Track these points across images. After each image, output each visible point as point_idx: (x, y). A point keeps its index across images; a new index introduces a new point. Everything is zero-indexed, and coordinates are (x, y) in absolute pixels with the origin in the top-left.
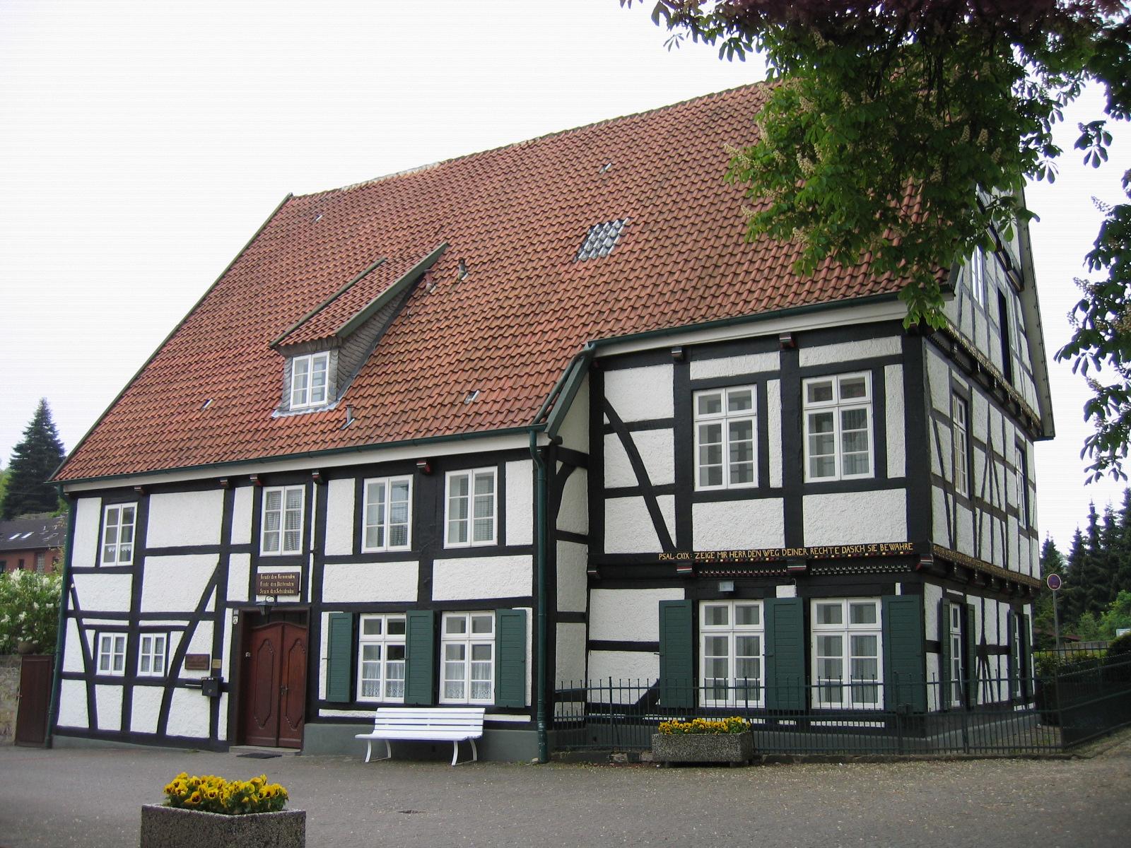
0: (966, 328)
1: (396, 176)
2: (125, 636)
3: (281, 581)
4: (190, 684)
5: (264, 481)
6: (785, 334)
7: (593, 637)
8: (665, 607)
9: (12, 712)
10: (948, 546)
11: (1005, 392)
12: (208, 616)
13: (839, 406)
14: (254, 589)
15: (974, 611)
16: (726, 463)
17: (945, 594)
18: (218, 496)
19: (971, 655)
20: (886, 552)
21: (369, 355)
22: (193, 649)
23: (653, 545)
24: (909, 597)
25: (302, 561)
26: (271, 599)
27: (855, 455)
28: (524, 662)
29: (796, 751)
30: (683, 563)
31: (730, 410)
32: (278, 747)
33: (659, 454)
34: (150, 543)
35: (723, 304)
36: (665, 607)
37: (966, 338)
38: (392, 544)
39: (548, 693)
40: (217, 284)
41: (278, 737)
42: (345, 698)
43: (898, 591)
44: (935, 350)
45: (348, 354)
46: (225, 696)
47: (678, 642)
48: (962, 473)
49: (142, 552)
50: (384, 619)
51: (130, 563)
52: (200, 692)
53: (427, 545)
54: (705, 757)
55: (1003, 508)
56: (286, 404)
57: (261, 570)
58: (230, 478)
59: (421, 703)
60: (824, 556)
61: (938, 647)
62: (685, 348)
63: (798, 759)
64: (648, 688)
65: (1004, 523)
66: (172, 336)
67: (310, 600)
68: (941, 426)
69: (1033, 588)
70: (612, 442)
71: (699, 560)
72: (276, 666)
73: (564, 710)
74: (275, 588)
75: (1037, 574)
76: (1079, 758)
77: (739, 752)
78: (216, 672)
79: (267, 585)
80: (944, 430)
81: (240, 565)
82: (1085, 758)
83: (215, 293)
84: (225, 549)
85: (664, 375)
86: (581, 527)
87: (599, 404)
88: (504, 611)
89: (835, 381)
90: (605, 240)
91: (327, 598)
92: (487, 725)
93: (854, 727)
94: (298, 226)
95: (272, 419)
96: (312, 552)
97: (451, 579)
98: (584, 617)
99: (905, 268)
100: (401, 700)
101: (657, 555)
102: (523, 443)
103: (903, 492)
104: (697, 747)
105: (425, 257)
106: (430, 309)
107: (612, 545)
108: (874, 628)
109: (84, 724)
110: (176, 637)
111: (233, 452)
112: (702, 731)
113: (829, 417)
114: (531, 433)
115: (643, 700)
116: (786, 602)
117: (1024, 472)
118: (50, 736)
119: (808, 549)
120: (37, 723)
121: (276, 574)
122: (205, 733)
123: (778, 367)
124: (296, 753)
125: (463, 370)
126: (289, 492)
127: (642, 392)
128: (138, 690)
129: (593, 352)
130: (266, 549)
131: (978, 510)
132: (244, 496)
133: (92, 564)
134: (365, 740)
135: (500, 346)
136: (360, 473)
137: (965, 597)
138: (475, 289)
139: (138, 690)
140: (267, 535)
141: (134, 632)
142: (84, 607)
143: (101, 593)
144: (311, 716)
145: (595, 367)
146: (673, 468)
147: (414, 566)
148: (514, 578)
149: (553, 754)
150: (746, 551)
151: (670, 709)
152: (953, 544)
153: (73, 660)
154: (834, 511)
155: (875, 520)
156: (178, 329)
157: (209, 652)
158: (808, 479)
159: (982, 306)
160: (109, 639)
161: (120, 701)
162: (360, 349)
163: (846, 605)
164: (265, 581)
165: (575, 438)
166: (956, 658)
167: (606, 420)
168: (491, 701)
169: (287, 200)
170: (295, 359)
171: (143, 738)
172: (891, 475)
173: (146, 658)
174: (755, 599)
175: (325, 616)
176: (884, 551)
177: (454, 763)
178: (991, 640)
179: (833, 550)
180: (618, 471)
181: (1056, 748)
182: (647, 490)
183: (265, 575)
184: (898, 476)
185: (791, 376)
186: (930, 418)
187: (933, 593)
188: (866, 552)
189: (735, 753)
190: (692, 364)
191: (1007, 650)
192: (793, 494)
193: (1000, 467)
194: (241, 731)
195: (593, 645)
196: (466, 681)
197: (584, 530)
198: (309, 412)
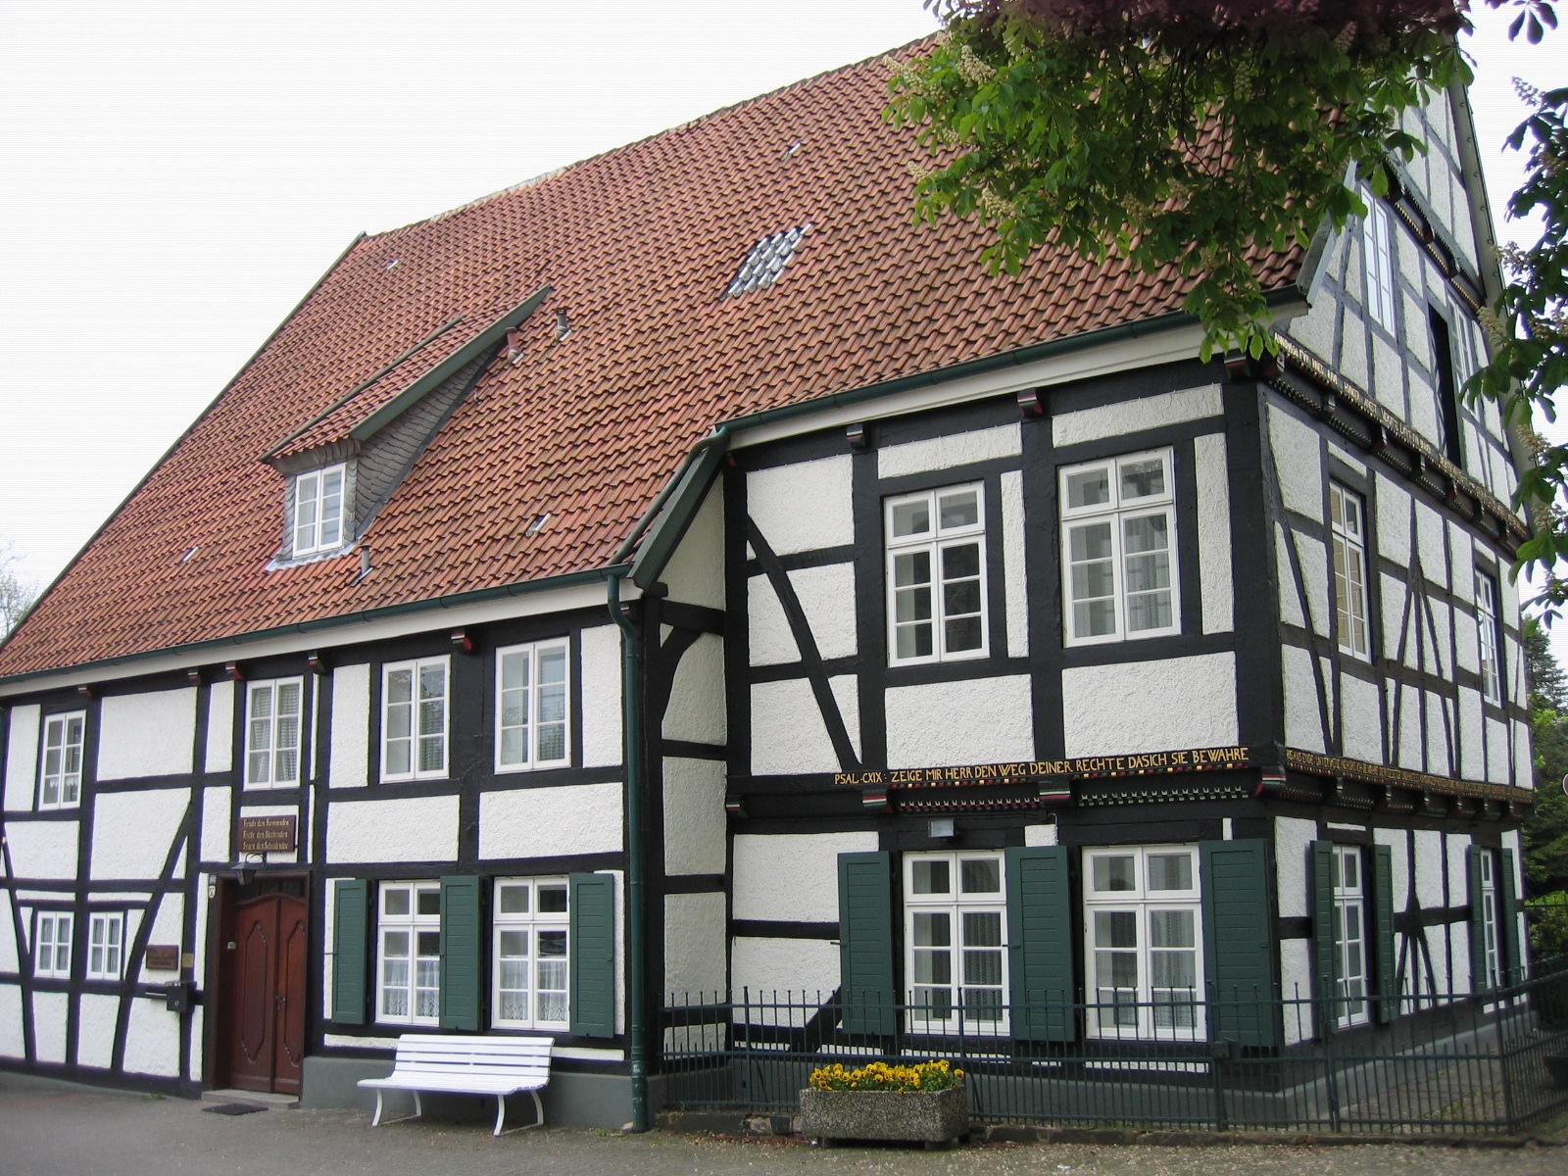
0: (1353, 366)
1: (504, 194)
4: (152, 992)
5: (247, 671)
6: (1026, 393)
8: (848, 864)
10: (1321, 748)
11: (1446, 480)
14: (235, 848)
15: (1388, 856)
16: (1119, 596)
17: (1322, 831)
18: (190, 695)
19: (1383, 932)
20: (1203, 765)
22: (156, 939)
23: (823, 760)
25: (297, 797)
26: (258, 859)
27: (1156, 595)
28: (613, 961)
29: (1043, 1120)
31: (943, 527)
32: (273, 1091)
33: (830, 602)
34: (103, 774)
35: (933, 349)
36: (848, 864)
37: (1354, 386)
39: (652, 1012)
40: (243, 372)
41: (274, 1077)
42: (356, 1017)
43: (1227, 833)
44: (1287, 404)
45: (375, 466)
46: (199, 1010)
47: (868, 924)
48: (1354, 615)
51: (76, 804)
52: (163, 1006)
53: (471, 774)
54: (884, 1130)
55: (1448, 676)
56: (287, 549)
57: (246, 812)
58: (202, 669)
59: (461, 1027)
60: (1099, 774)
61: (1303, 928)
62: (869, 426)
63: (1044, 1134)
64: (818, 1006)
65: (1450, 702)
66: (170, 454)
67: (310, 861)
68: (1300, 538)
69: (1516, 803)
70: (760, 589)
71: (898, 784)
73: (677, 1040)
75: (1525, 779)
76: (1541, 1144)
77: (939, 1125)
78: (188, 973)
79: (252, 835)
80: (1312, 551)
81: (217, 800)
82: (1551, 1144)
83: (238, 386)
84: (198, 780)
86: (715, 732)
87: (740, 528)
88: (582, 877)
89: (1112, 468)
90: (773, 261)
91: (333, 857)
92: (557, 1065)
93: (1158, 1072)
94: (369, 271)
95: (266, 574)
96: (312, 782)
97: (514, 826)
98: (723, 883)
99: (1194, 257)
100: (434, 1022)
101: (831, 776)
102: (596, 597)
103: (1229, 657)
104: (871, 1113)
106: (507, 391)
107: (763, 763)
108: (1189, 898)
110: (135, 917)
112: (883, 1084)
114: (610, 579)
115: (811, 1026)
116: (1041, 853)
117: (1495, 612)
119: (1073, 762)
121: (264, 819)
122: (172, 1070)
123: (1018, 450)
124: (291, 1106)
125: (534, 482)
126: (283, 688)
127: (803, 504)
128: (87, 1000)
129: (726, 439)
131: (1391, 683)
132: (222, 695)
133: (28, 807)
134: (372, 1091)
135: (593, 440)
136: (374, 654)
137: (1370, 834)
138: (646, 358)
139: (87, 1000)
141: (82, 910)
142: (18, 873)
145: (729, 466)
146: (854, 629)
147: (452, 802)
148: (593, 820)
149: (658, 1116)
150: (972, 768)
151: (1053, 1044)
152: (1334, 744)
154: (1114, 695)
155: (1183, 710)
156: (179, 444)
158: (1072, 641)
159: (1393, 334)
160: (102, 921)
162: (397, 458)
163: (1140, 859)
164: (249, 830)
165: (694, 580)
166: (1349, 941)
167: (751, 554)
168: (563, 1026)
169: (357, 242)
170: (300, 478)
171: (92, 1076)
172: (1208, 629)
173: (97, 951)
174: (992, 848)
175: (330, 885)
176: (1199, 763)
177: (497, 1131)
178: (1430, 897)
179: (1114, 763)
180: (770, 639)
181: (1497, 1123)
182: (813, 668)
183: (249, 820)
185: (1041, 464)
186: (1278, 525)
187: (1294, 835)
188: (1169, 765)
189: (930, 1125)
190: (881, 452)
191: (1467, 914)
192: (1046, 666)
193: (1440, 608)
194: (223, 1068)
195: (738, 928)
197: (718, 738)
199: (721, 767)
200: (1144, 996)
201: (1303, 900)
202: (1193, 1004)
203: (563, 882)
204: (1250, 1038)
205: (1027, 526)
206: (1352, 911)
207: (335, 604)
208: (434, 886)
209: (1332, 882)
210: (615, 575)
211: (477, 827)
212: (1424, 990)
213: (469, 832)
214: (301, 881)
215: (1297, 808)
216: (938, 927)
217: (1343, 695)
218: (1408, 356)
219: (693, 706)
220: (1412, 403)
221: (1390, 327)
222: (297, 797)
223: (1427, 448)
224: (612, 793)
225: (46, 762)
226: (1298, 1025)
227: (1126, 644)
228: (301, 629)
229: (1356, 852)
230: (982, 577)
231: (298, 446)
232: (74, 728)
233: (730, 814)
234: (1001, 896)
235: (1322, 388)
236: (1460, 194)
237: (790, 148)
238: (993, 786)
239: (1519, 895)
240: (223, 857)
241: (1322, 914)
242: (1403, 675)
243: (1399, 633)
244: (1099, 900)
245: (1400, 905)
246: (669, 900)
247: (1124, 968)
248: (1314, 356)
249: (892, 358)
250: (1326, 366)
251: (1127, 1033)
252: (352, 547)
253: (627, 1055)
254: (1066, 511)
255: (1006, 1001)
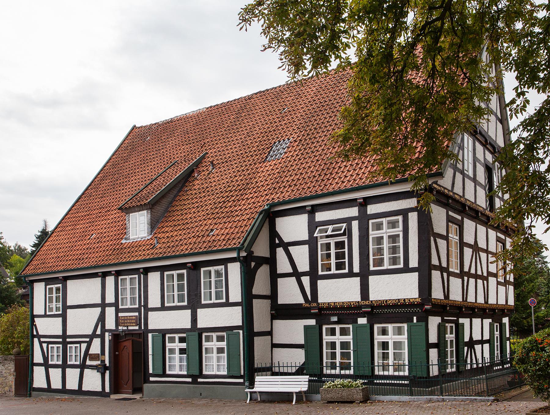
0: (458, 189)
2: (61, 346)
3: (129, 319)
5: (118, 274)
6: (360, 199)
7: (274, 342)
8: (306, 328)
9: (12, 382)
12: (98, 336)
13: (386, 233)
14: (117, 324)
16: (386, 256)
17: (443, 320)
18: (98, 280)
19: (461, 347)
21: (167, 211)
23: (299, 300)
24: (420, 323)
25: (138, 310)
26: (126, 328)
28: (240, 355)
30: (314, 308)
33: (301, 256)
36: (306, 328)
37: (458, 195)
38: (216, 299)
42: (160, 372)
43: (415, 321)
46: (108, 372)
49: (65, 308)
50: (177, 336)
53: (194, 304)
57: (120, 314)
65: (485, 282)
67: (143, 328)
69: (507, 310)
70: (280, 251)
72: (129, 358)
74: (127, 323)
75: (511, 302)
80: (442, 244)
81: (110, 312)
83: (98, 179)
84: (103, 305)
85: (304, 218)
88: (230, 332)
89: (384, 220)
91: (150, 327)
94: (140, 142)
95: (122, 244)
97: (207, 318)
98: (270, 333)
102: (234, 255)
105: (195, 160)
106: (197, 187)
107: (281, 300)
108: (404, 338)
109: (45, 386)
110: (84, 346)
111: (103, 260)
113: (382, 238)
116: (362, 326)
118: (30, 391)
119: (372, 301)
120: (24, 386)
121: (127, 317)
122: (99, 389)
123: (357, 215)
125: (209, 219)
126: (131, 278)
127: (293, 228)
129: (269, 209)
130: (122, 305)
131: (466, 278)
132: (110, 281)
136: (162, 269)
137: (458, 320)
140: (122, 299)
141: (65, 344)
142: (41, 333)
143: (48, 327)
144: (147, 381)
145: (271, 216)
147: (189, 312)
148: (233, 317)
151: (365, 376)
152: (447, 296)
153: (38, 358)
155: (400, 288)
157: (99, 352)
161: (61, 375)
163: (390, 327)
164: (122, 320)
165: (261, 249)
167: (277, 241)
169: (133, 129)
171: (56, 391)
172: (411, 266)
173: (71, 356)
174: (348, 324)
175: (150, 335)
177: (294, 403)
178: (477, 336)
180: (283, 266)
182: (296, 274)
183: (122, 317)
184: (414, 266)
185: (364, 219)
187: (434, 322)
192: (364, 275)
193: (483, 255)
194: (116, 388)
195: (274, 346)
196: (214, 364)
198: (139, 240)
199: (269, 301)
200: (391, 363)
201: (436, 338)
202: (404, 365)
203: (224, 334)
204: (419, 374)
205: (359, 236)
206: (497, 337)
207: (148, 254)
208: (184, 335)
209: (445, 333)
210: (239, 250)
211: (196, 319)
212: (474, 362)
213: (194, 320)
214: (140, 334)
215: (435, 314)
216: (333, 345)
217: (450, 282)
218: (477, 182)
219: (261, 285)
220: (477, 196)
221: (471, 174)
222: (138, 310)
223: (481, 209)
224: (238, 310)
225: (48, 300)
226: (434, 371)
227: (387, 269)
228: (137, 262)
229: (454, 325)
230: (346, 250)
231: (130, 205)
232: (58, 289)
233: (272, 314)
234: (351, 337)
235: (448, 197)
236: (500, 126)
237: (284, 109)
238: (349, 307)
239: (508, 336)
240: (113, 327)
241: (442, 342)
242: (469, 275)
243: (469, 264)
244: (379, 338)
245: (467, 339)
246: (255, 338)
247: (385, 356)
248: (445, 188)
249: (319, 186)
250: (449, 191)
251: (386, 373)
252: (150, 237)
253: (244, 381)
254: (371, 232)
255: (352, 365)
